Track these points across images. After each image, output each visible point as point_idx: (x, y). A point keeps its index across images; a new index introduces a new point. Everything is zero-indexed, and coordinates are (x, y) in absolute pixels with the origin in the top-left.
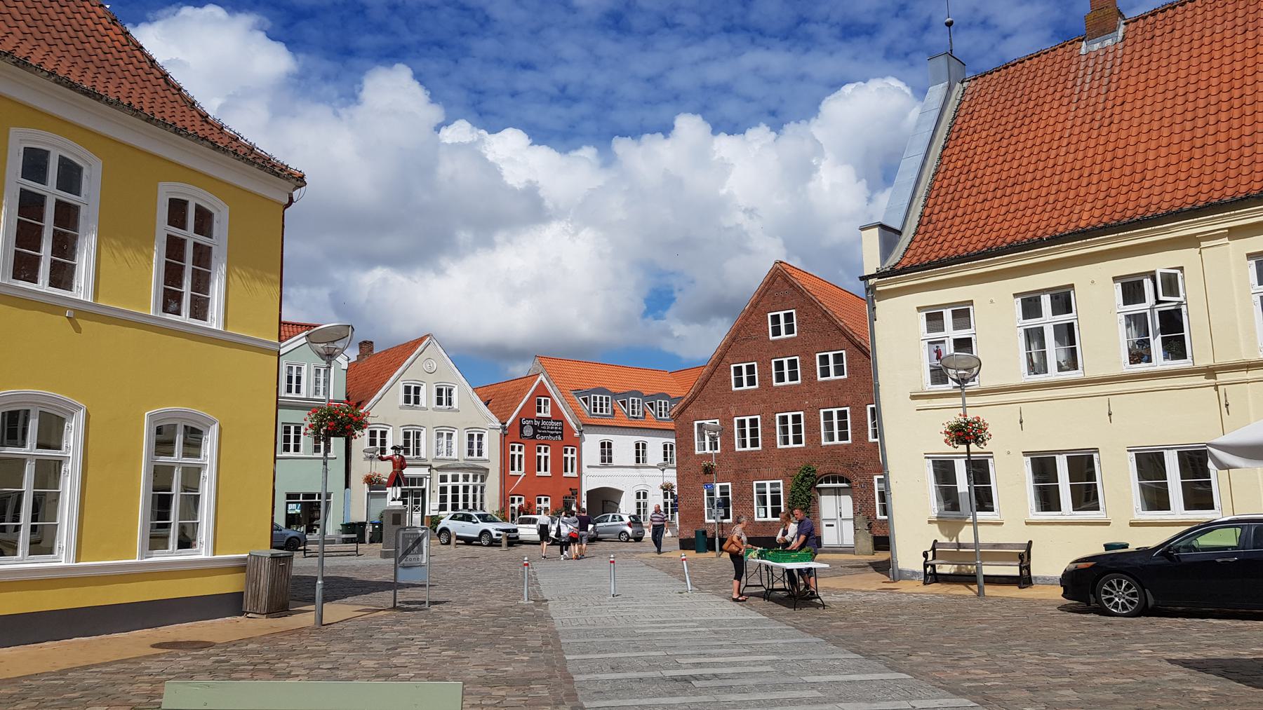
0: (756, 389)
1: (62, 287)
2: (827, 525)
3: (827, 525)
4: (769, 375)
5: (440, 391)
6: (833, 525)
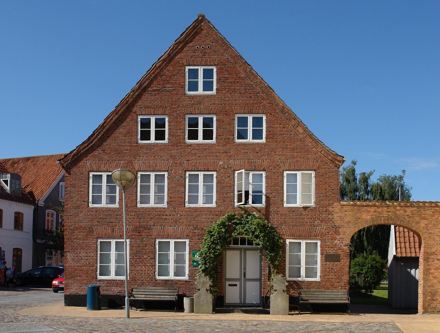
0: (165, 145)
1: (95, 203)
2: (230, 285)
3: (230, 285)
4: (182, 131)
6: (236, 285)
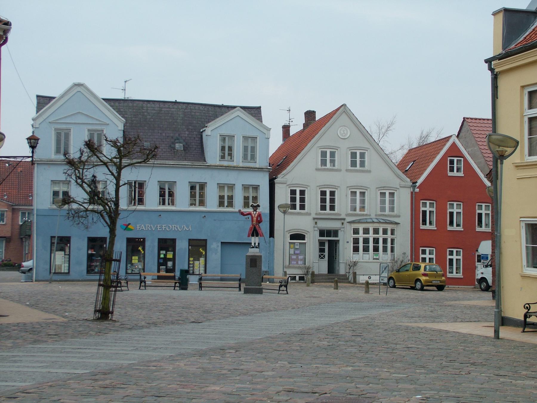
5: (354, 155)
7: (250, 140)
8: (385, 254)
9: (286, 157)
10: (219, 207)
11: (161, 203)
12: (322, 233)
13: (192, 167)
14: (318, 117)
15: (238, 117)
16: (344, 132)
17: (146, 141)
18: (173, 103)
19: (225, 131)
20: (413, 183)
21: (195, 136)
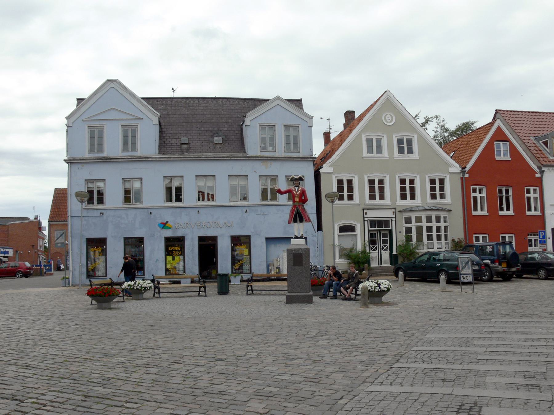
7: (291, 129)
8: (439, 243)
9: (330, 152)
10: (262, 200)
11: (201, 199)
12: (372, 223)
13: (230, 159)
14: (357, 116)
15: (278, 106)
16: (389, 118)
17: (183, 136)
18: (212, 99)
19: (264, 120)
20: (462, 169)
21: (234, 129)
